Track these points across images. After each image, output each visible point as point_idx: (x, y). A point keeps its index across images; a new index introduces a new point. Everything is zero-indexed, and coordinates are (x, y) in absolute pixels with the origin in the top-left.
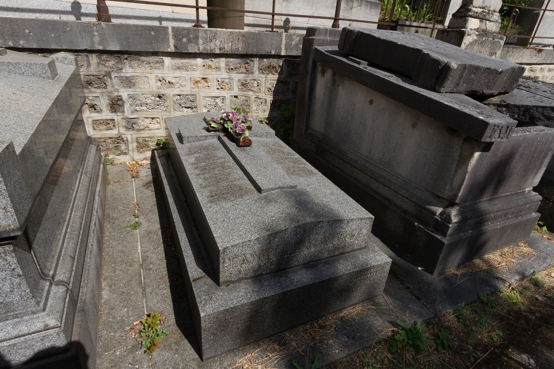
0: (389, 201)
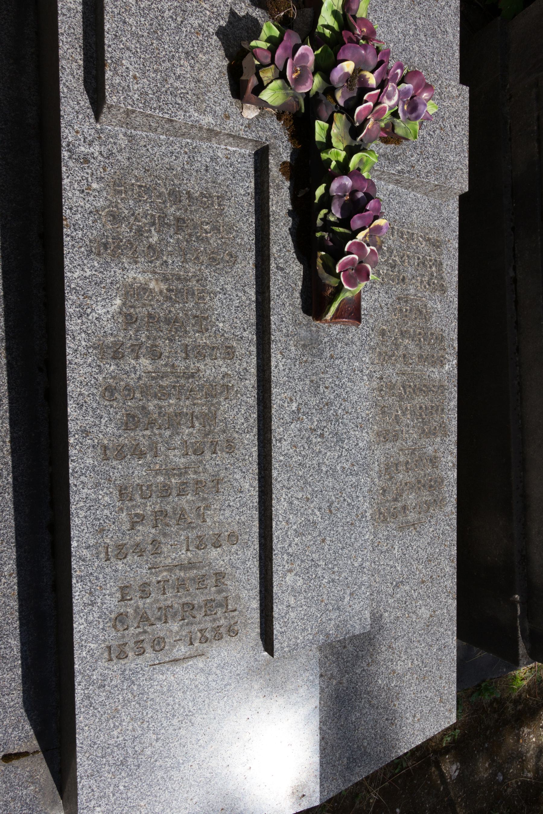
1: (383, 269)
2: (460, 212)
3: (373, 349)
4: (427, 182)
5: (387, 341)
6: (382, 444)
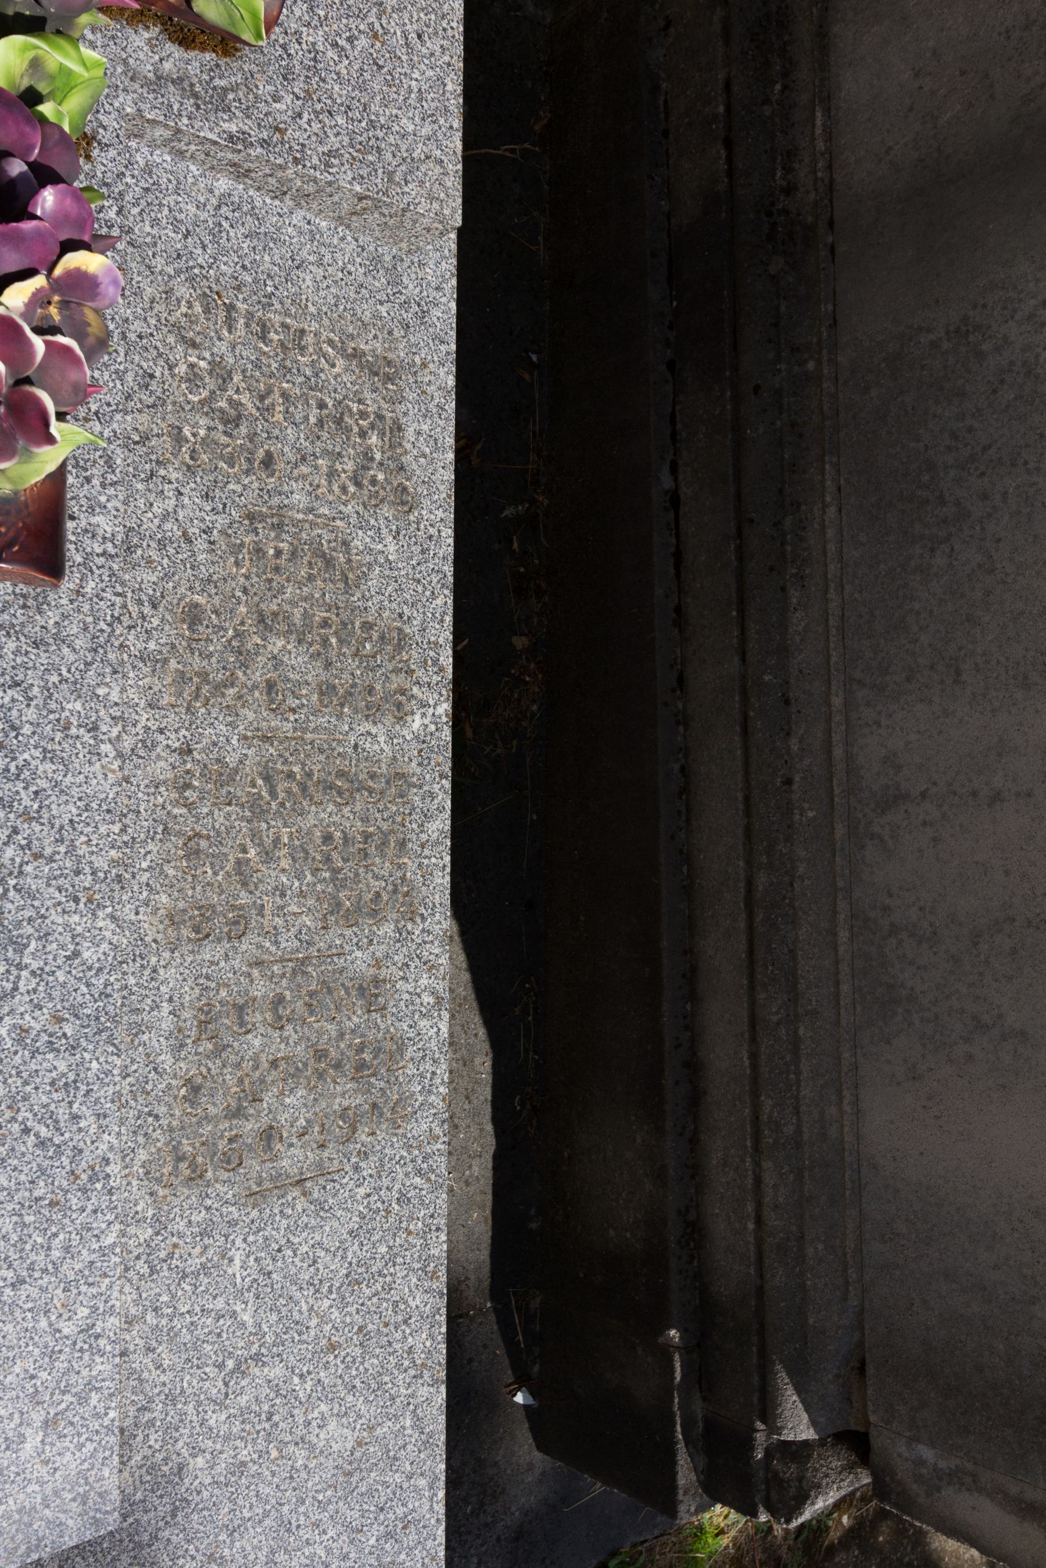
0: (695, 1099)
1: (196, 425)
2: (461, 288)
3: (156, 662)
4: (330, 184)
5: (208, 640)
6: (186, 948)
